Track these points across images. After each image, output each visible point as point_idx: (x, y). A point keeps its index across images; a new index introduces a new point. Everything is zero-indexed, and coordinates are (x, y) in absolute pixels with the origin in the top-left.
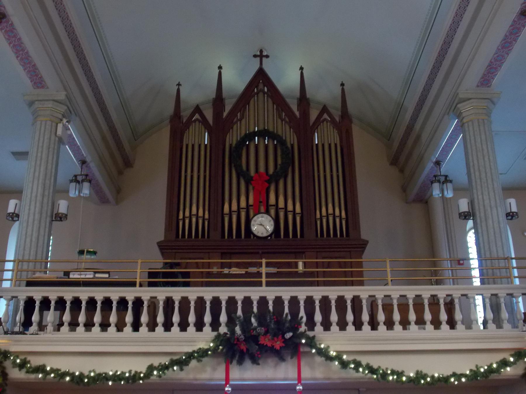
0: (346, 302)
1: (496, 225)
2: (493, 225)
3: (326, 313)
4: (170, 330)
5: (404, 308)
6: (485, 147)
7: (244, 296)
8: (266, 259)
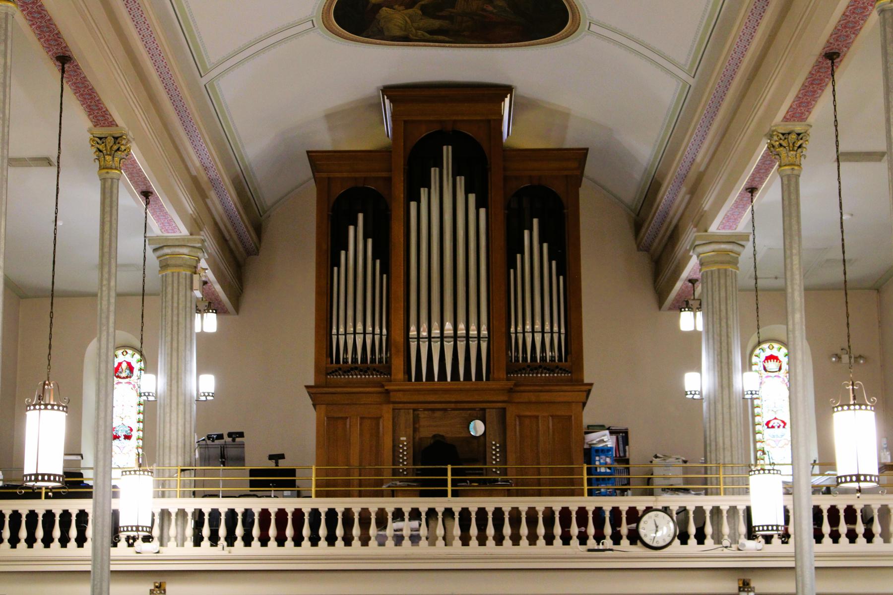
0: (503, 513)
1: (726, 410)
2: (723, 410)
3: (331, 526)
4: (535, 544)
5: (532, 521)
6: (723, 307)
7: (119, 510)
8: (452, 465)
